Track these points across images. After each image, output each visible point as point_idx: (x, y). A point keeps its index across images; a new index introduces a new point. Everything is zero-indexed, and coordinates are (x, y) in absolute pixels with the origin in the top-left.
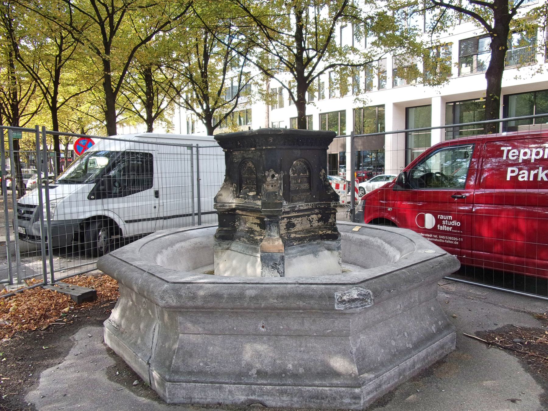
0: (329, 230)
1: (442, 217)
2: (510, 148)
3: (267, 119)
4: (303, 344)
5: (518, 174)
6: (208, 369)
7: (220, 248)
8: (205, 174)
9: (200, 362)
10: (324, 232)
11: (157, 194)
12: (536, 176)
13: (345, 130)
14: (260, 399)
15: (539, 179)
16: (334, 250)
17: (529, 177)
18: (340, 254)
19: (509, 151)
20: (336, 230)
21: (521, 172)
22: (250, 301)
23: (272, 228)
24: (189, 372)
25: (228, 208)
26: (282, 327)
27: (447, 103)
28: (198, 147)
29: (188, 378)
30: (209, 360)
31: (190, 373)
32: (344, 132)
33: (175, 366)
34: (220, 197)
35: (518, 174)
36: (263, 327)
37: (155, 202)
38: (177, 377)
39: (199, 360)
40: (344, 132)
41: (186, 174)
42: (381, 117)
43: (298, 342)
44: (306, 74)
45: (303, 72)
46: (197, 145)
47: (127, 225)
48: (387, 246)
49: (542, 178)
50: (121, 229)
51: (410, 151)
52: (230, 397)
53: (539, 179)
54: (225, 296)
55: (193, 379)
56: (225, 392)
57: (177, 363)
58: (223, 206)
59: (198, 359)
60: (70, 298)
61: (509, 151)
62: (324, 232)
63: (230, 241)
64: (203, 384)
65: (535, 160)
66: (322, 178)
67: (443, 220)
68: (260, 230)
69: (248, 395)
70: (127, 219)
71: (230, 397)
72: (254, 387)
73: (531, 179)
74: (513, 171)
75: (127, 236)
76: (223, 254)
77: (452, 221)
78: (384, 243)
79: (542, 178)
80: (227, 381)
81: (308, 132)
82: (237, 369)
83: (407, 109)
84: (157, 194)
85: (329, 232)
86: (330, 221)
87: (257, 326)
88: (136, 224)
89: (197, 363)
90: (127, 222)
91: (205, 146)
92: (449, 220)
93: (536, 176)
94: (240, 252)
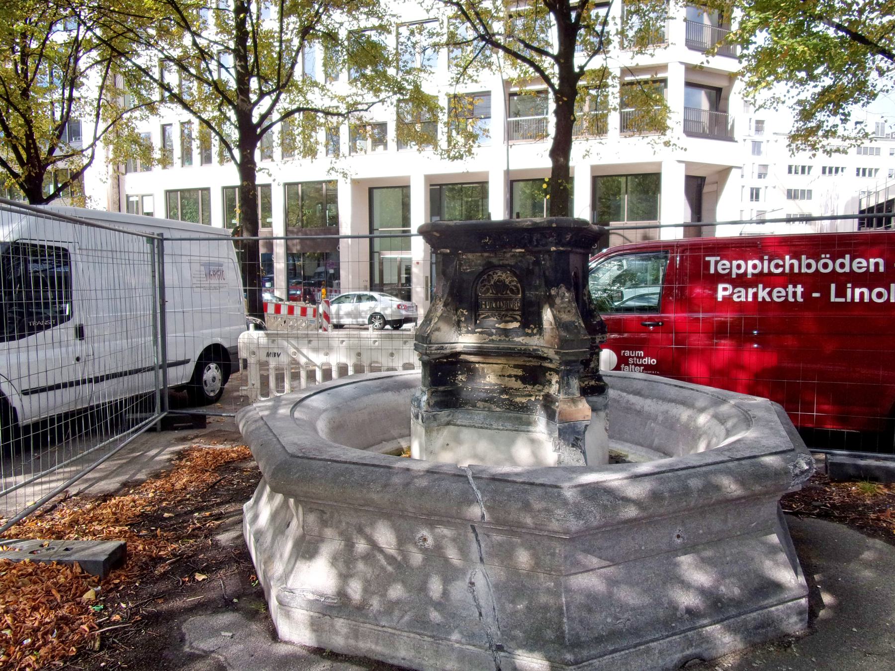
0: (592, 379)
1: (627, 353)
2: (718, 258)
3: (116, 190)
4: (728, 552)
5: (733, 293)
6: (621, 626)
7: (435, 424)
8: (177, 291)
9: (606, 617)
10: (586, 383)
11: (80, 332)
12: (755, 295)
13: (270, 216)
14: (698, 650)
15: (760, 299)
16: (600, 410)
17: (747, 297)
18: (607, 415)
19: (717, 263)
20: (599, 378)
21: (736, 290)
22: (699, 496)
23: (571, 381)
24: (596, 638)
25: (448, 351)
26: (701, 532)
27: (431, 185)
28: (162, 240)
29: (600, 649)
30: (618, 610)
31: (599, 640)
32: (268, 220)
33: (572, 635)
34: (437, 333)
35: (733, 293)
36: (678, 536)
37: (80, 348)
38: (585, 653)
39: (604, 613)
40: (268, 220)
41: (99, 293)
42: (332, 199)
43: (721, 550)
44: (255, 120)
45: (250, 116)
46: (162, 234)
47: (26, 398)
48: (632, 398)
49: (763, 298)
50: (14, 408)
51: (376, 255)
52: (660, 661)
53: (760, 299)
54: (667, 494)
55: (611, 648)
56: (654, 654)
57: (573, 629)
58: (442, 348)
59: (602, 612)
60: (79, 570)
61: (717, 263)
62: (586, 383)
63: (452, 410)
64: (623, 653)
65: (753, 274)
66: (585, 298)
67: (630, 357)
68: (522, 386)
69: (682, 651)
70: (25, 387)
71: (660, 661)
72: (689, 634)
73: (750, 299)
74: (725, 289)
75: (26, 422)
76: (440, 433)
77: (643, 358)
78: (625, 394)
79: (763, 298)
80: (657, 636)
81: (483, 225)
82: (661, 613)
83: (371, 190)
84: (80, 332)
85: (593, 383)
86: (592, 365)
87: (671, 538)
88: (43, 395)
89: (602, 620)
90: (25, 393)
91: (179, 237)
92: (639, 358)
93: (755, 295)
94: (481, 428)
